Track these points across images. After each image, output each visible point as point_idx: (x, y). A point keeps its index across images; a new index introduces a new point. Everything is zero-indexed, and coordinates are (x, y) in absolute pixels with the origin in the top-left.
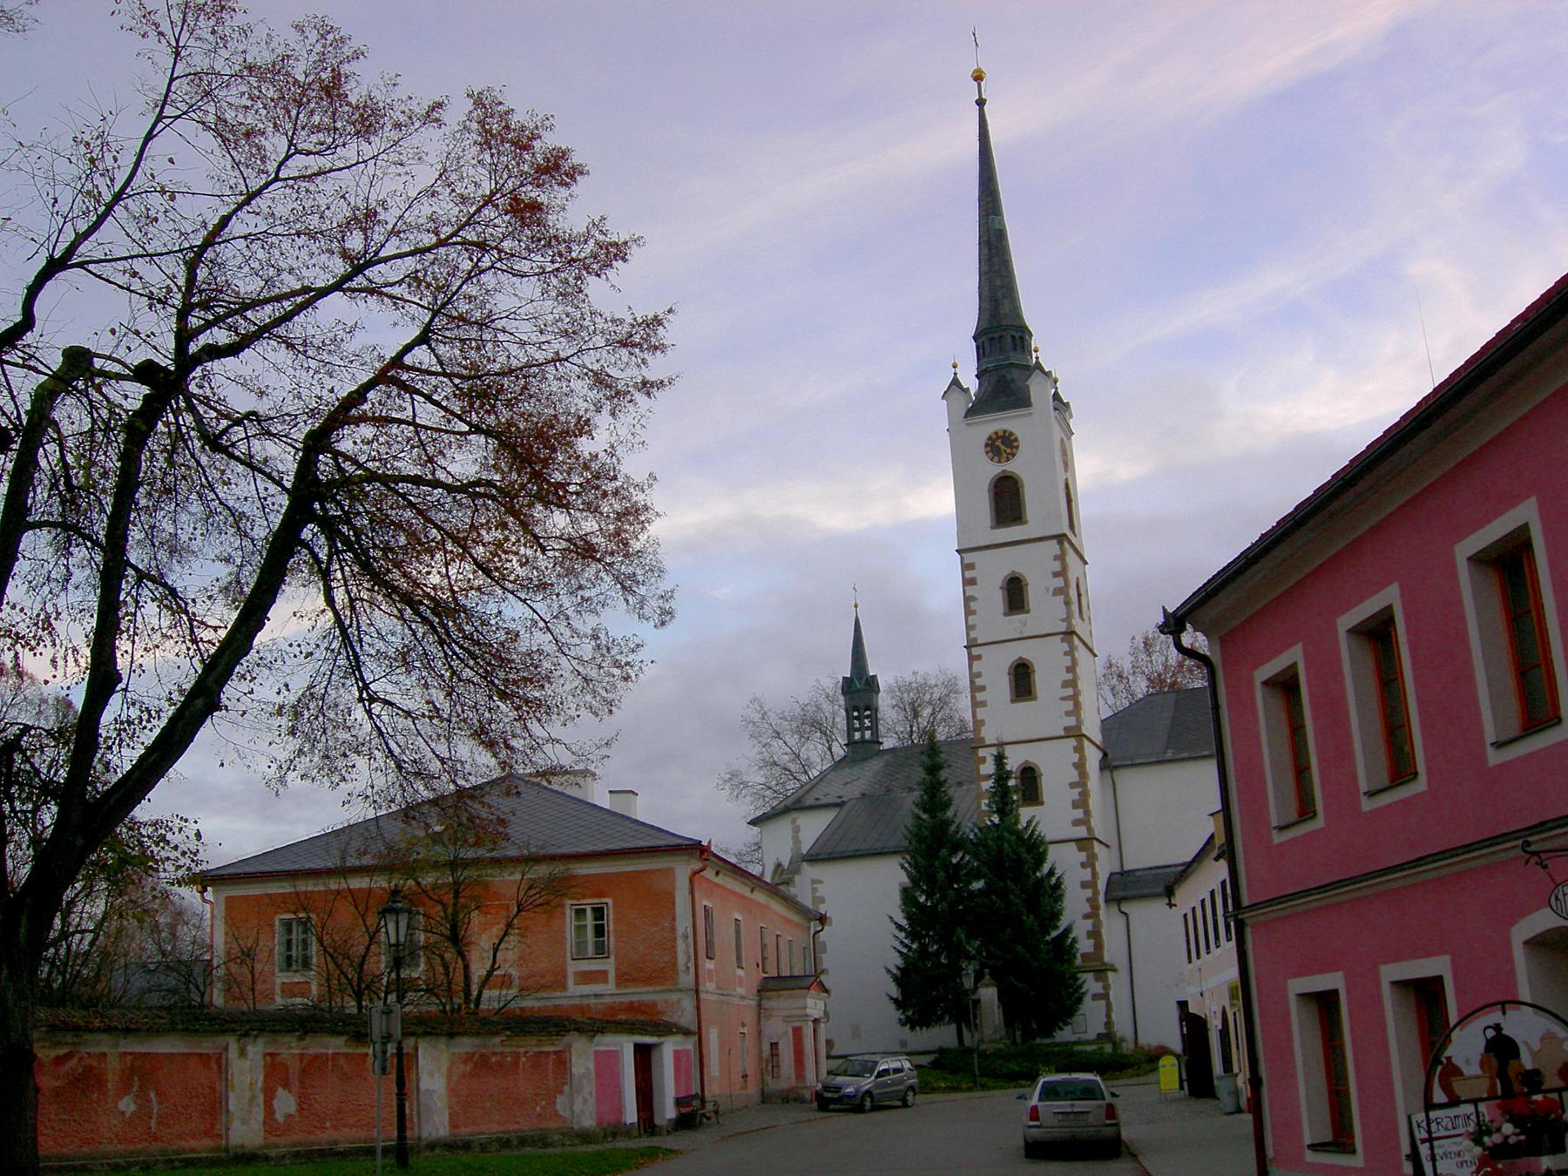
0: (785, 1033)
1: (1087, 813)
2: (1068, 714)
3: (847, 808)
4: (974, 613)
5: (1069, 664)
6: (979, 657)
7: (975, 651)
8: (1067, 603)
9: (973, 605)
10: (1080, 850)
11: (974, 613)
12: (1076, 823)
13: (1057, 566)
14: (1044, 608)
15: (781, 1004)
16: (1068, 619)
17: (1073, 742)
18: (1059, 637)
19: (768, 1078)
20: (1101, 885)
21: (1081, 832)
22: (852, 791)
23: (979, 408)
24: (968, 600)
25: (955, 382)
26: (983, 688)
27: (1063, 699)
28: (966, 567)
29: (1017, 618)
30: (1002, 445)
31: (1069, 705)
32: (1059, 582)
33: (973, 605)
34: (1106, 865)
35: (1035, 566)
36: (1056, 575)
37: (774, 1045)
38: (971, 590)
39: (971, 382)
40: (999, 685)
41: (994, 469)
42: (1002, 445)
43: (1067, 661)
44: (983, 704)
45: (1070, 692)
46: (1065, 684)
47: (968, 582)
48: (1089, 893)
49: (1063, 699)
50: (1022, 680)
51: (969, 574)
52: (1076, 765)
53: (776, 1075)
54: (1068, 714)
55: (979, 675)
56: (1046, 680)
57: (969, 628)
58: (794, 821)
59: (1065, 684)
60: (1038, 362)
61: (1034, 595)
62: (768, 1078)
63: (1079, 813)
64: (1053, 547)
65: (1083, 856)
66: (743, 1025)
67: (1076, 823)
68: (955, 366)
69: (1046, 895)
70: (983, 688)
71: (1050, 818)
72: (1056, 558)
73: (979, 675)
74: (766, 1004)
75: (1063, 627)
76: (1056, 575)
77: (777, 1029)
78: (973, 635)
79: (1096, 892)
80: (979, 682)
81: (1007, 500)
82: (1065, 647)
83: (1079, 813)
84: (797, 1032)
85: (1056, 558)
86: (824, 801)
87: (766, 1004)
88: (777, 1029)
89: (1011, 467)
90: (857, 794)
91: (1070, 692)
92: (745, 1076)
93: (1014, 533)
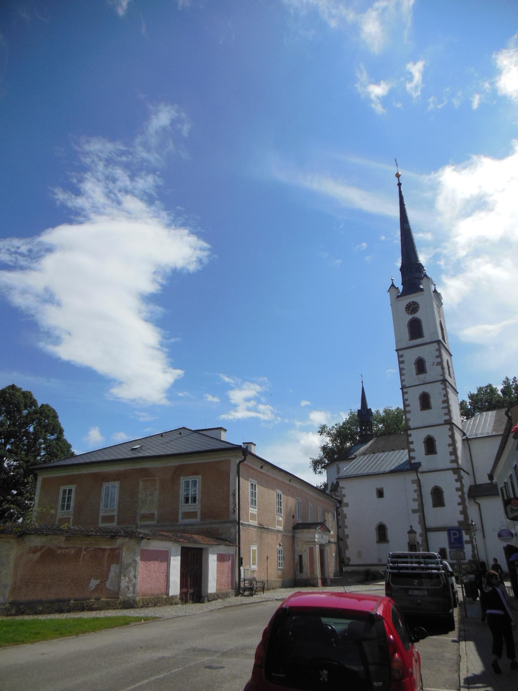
1: (457, 457)
4: (404, 375)
5: (445, 393)
6: (407, 393)
7: (405, 390)
8: (443, 368)
11: (404, 375)
14: (432, 372)
15: (304, 535)
16: (443, 374)
17: (448, 426)
18: (440, 383)
19: (298, 573)
20: (466, 490)
21: (454, 465)
24: (401, 370)
26: (409, 405)
27: (443, 408)
28: (400, 356)
29: (422, 376)
30: (412, 308)
31: (446, 411)
32: (439, 360)
33: (403, 372)
34: (467, 482)
37: (301, 557)
38: (402, 366)
40: (415, 404)
41: (410, 317)
42: (412, 308)
45: (446, 405)
47: (400, 362)
48: (460, 493)
49: (443, 408)
50: (425, 402)
51: (401, 359)
52: (460, 496)
53: (301, 571)
54: (446, 414)
55: (407, 400)
57: (402, 381)
58: (338, 466)
61: (428, 365)
63: (453, 458)
65: (456, 477)
70: (409, 405)
73: (407, 400)
75: (441, 378)
78: (404, 383)
79: (463, 493)
80: (407, 403)
81: (415, 329)
82: (443, 386)
83: (453, 458)
84: (311, 550)
85: (437, 350)
89: (417, 315)
91: (446, 405)
93: (419, 341)
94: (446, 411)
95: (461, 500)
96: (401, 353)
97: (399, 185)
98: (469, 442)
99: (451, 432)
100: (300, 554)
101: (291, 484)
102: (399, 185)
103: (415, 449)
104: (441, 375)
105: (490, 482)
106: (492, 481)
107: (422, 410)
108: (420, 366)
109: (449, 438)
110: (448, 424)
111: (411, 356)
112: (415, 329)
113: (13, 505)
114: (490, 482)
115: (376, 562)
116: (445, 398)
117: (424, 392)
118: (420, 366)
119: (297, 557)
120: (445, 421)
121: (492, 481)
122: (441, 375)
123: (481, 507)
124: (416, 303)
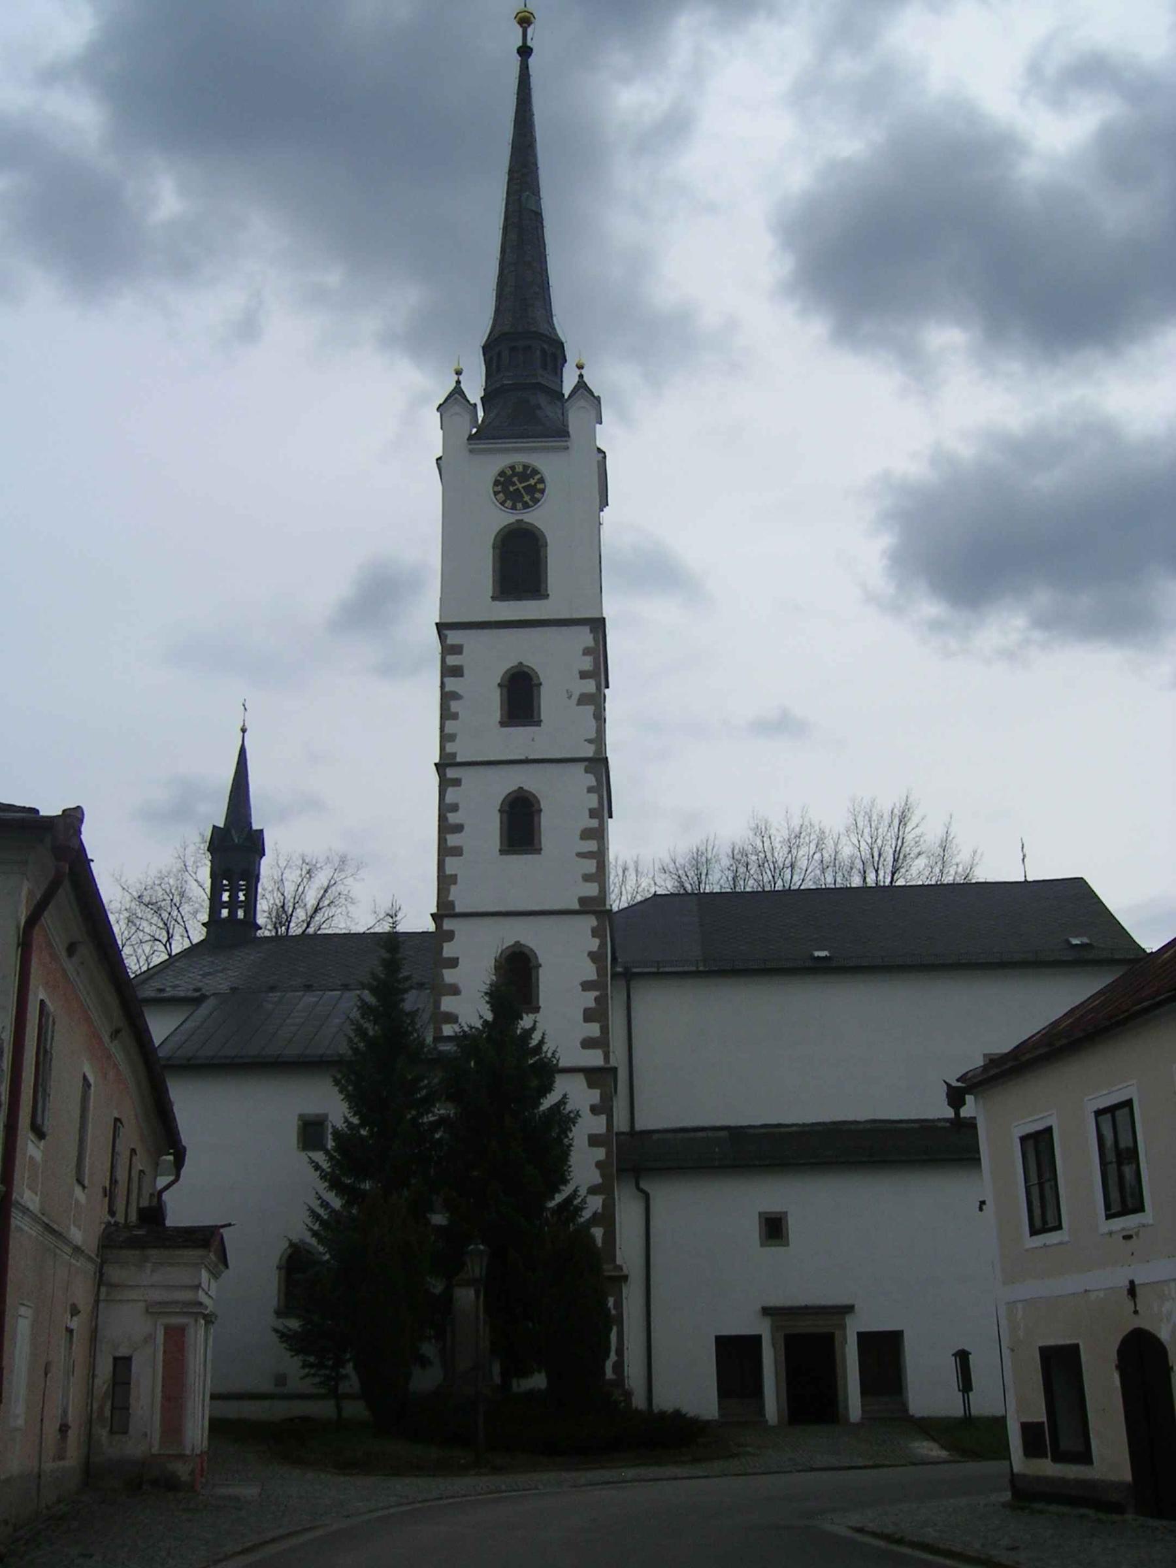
0: (149, 1338)
2: (587, 878)
3: (203, 1010)
4: (455, 716)
6: (457, 782)
7: (451, 773)
9: (454, 706)
10: (591, 1085)
11: (455, 716)
12: (588, 1044)
13: (587, 664)
14: (484, 797)
17: (592, 921)
18: (581, 767)
19: (103, 1433)
21: (595, 1058)
22: (220, 983)
23: (483, 437)
24: (447, 697)
25: (457, 393)
26: (459, 828)
27: (580, 855)
28: (448, 650)
30: (519, 488)
31: (590, 866)
33: (454, 706)
35: (554, 660)
36: (584, 675)
37: (122, 1364)
38: (453, 684)
39: (474, 392)
41: (503, 518)
42: (519, 488)
43: (593, 801)
44: (457, 852)
45: (592, 846)
46: (586, 834)
47: (449, 672)
49: (580, 855)
51: (452, 660)
54: (587, 878)
55: (455, 808)
56: (558, 824)
59: (586, 834)
60: (582, 386)
62: (103, 1433)
63: (594, 1029)
64: (585, 637)
65: (594, 1096)
66: (75, 1311)
67: (588, 1044)
68: (459, 373)
69: (548, 1140)
70: (459, 828)
71: (559, 1022)
72: (587, 652)
73: (455, 808)
74: (115, 1274)
75: (589, 751)
76: (584, 675)
77: (130, 1325)
78: (450, 748)
80: (453, 818)
81: (520, 564)
83: (594, 1029)
84: (176, 1339)
85: (587, 652)
86: (170, 992)
87: (115, 1274)
88: (130, 1325)
89: (535, 517)
90: (224, 987)
91: (592, 846)
92: (64, 1429)
94: (590, 866)
95: (603, 1176)
96: (454, 637)
97: (525, 52)
98: (633, 984)
99: (597, 941)
100: (123, 1352)
101: (1119, 1278)
102: (525, 52)
103: (461, 986)
104: (590, 741)
105: (950, 1113)
106: (957, 1113)
107: (502, 852)
108: (520, 697)
109: (588, 961)
110: (594, 913)
111: (490, 659)
112: (520, 564)
113: (431, 1123)
114: (950, 1113)
115: (267, 1386)
116: (594, 823)
117: (521, 788)
118: (520, 697)
119: (105, 1369)
120: (583, 901)
121: (957, 1113)
122: (590, 741)
123: (652, 1202)
124: (535, 472)
